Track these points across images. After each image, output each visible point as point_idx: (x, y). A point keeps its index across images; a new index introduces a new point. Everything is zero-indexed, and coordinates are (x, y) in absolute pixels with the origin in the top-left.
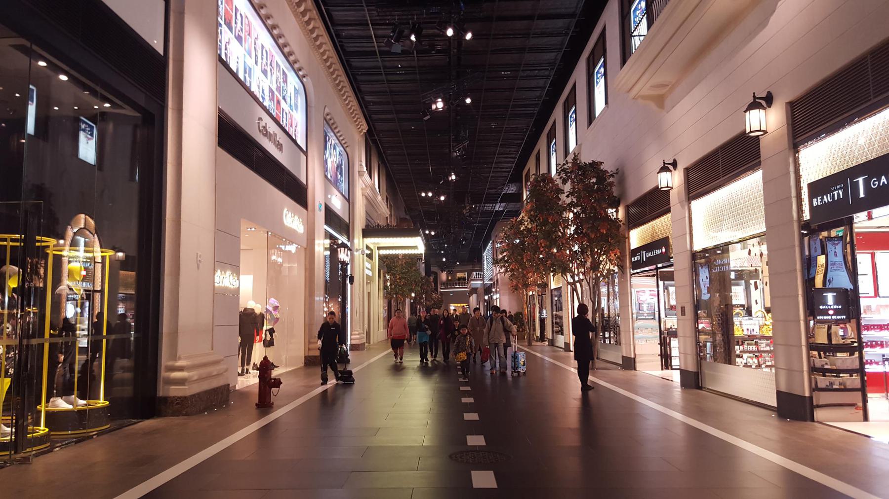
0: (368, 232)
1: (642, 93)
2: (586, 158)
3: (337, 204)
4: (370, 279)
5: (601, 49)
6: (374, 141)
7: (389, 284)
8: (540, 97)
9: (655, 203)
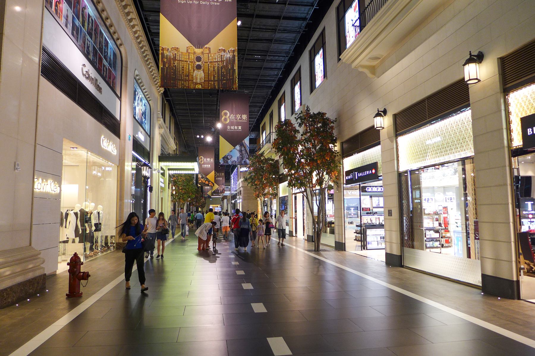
0: (163, 158)
1: (362, 63)
2: (314, 110)
3: (141, 137)
4: (163, 189)
5: (322, 43)
6: (167, 100)
7: (174, 193)
8: (277, 75)
9: (368, 138)
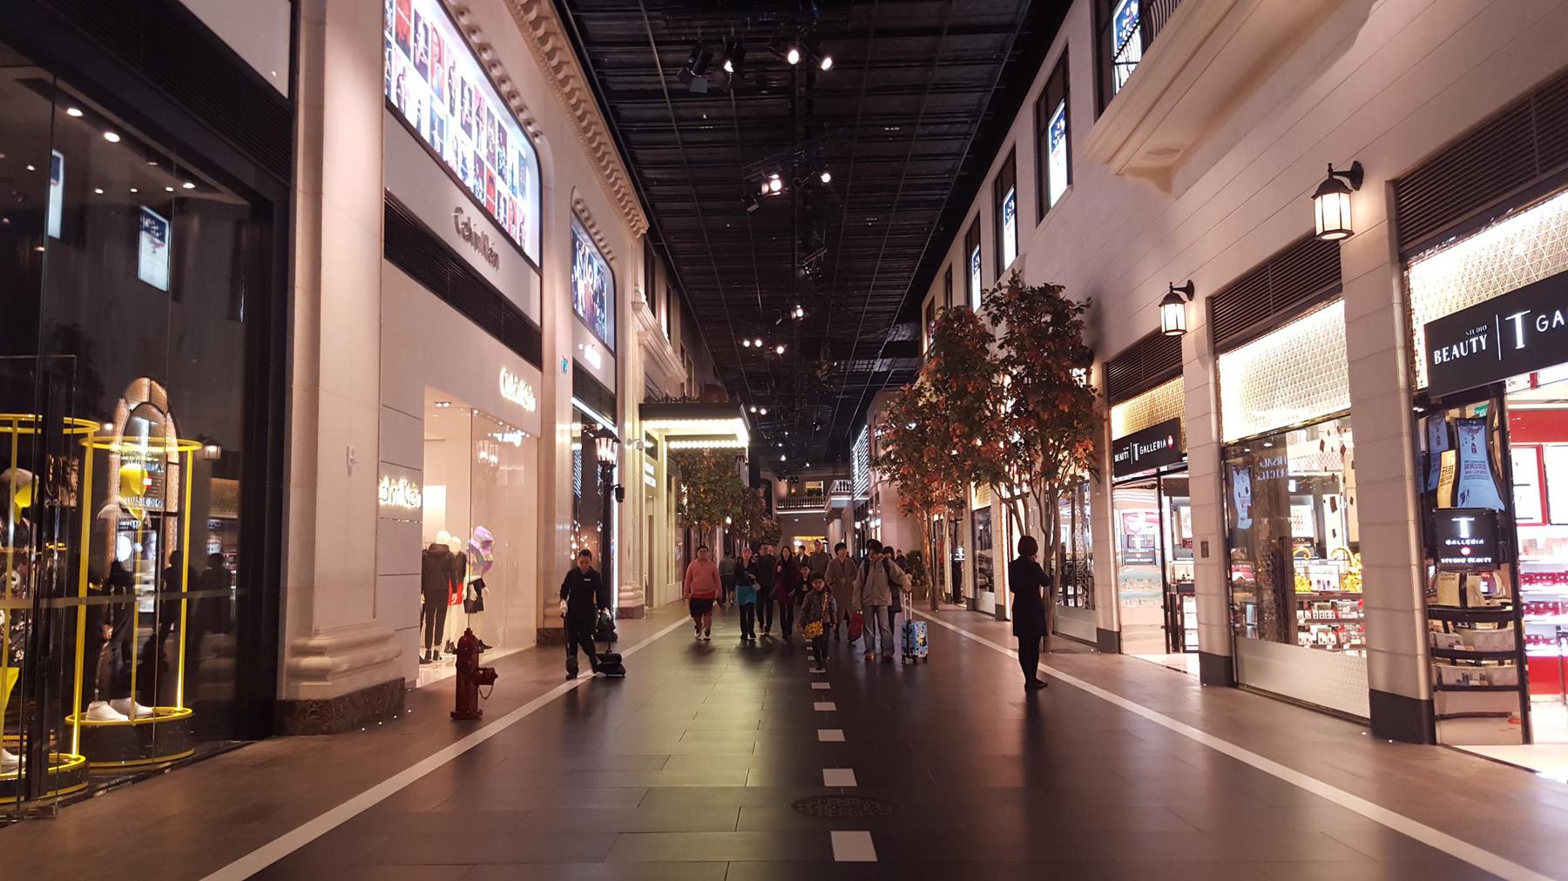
0: (649, 410)
1: (1132, 164)
2: (1033, 280)
3: (595, 359)
4: (652, 493)
5: (1059, 87)
6: (660, 250)
7: (685, 501)
8: (953, 171)
9: (1156, 359)
